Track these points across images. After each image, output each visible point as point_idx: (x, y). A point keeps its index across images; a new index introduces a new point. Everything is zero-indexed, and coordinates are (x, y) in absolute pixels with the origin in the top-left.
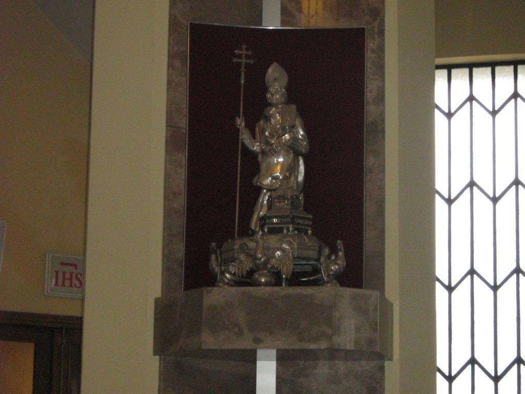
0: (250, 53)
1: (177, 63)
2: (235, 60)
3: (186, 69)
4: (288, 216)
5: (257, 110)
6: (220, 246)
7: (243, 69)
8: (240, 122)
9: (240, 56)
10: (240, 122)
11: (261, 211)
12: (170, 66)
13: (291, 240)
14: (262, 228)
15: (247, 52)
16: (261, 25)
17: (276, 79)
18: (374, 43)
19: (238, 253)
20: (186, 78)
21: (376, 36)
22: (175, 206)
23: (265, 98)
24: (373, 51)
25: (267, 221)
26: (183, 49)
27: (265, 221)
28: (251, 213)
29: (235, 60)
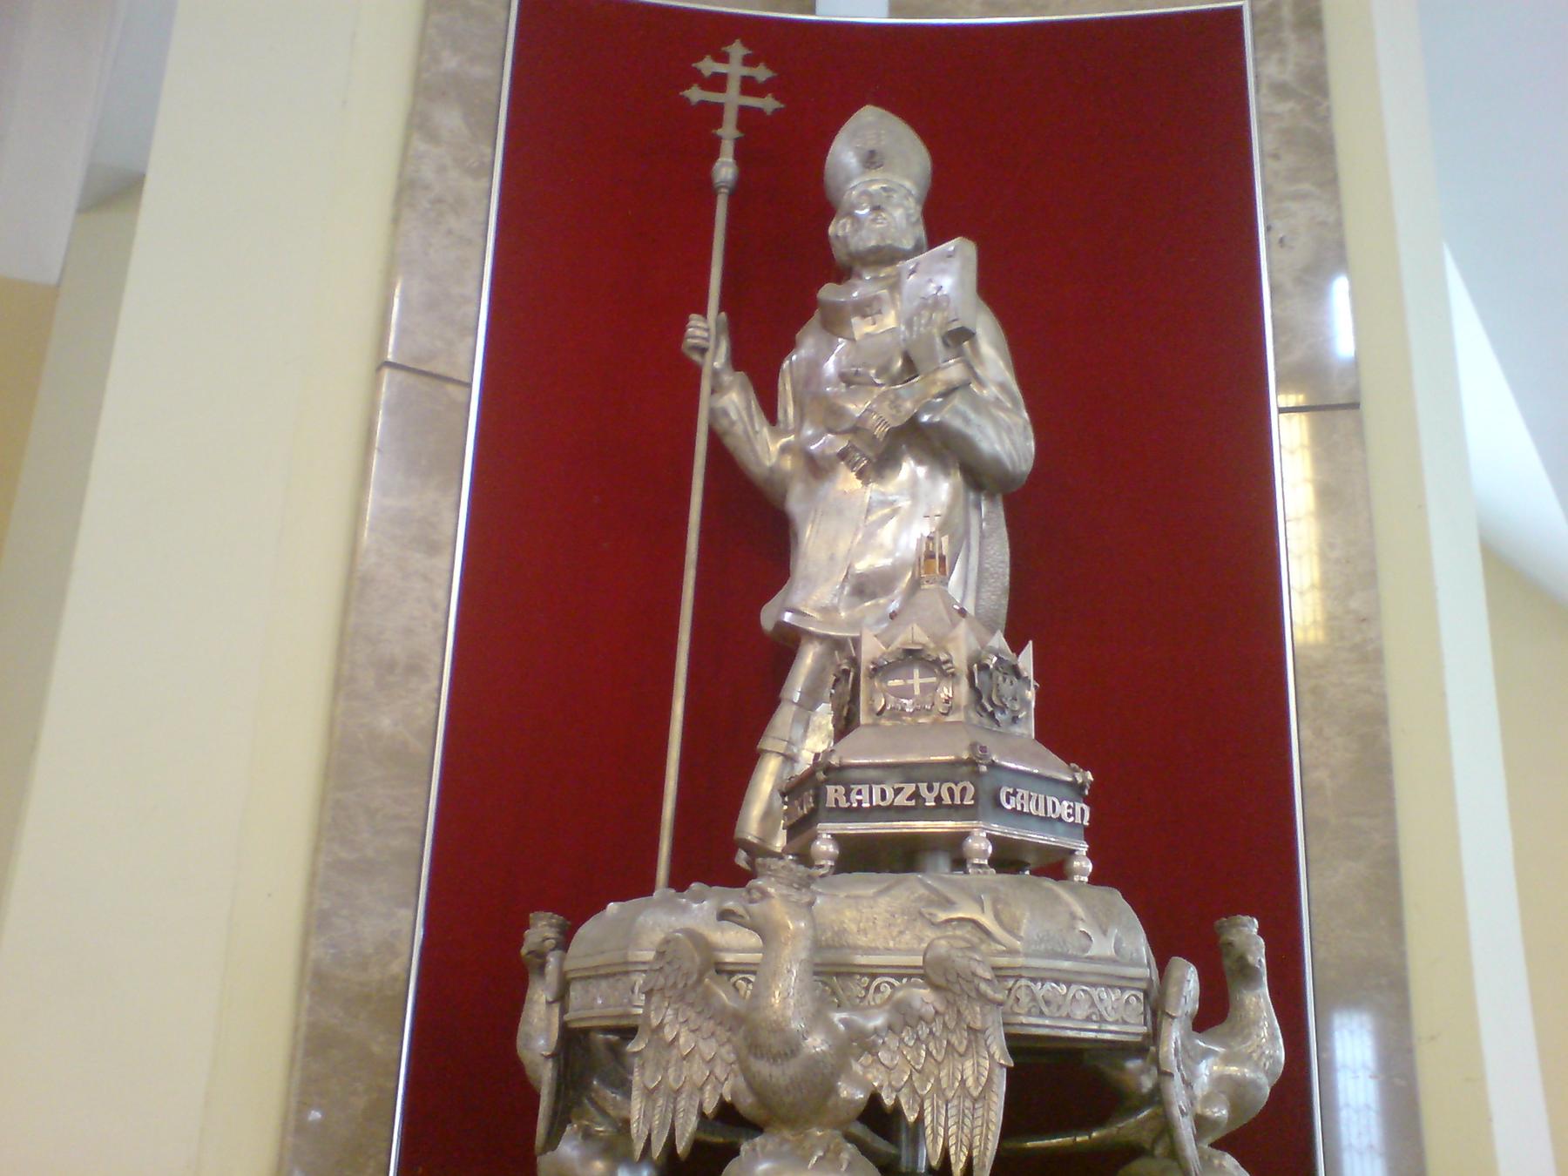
0: (762, 73)
1: (450, 119)
2: (695, 94)
3: (489, 151)
4: (949, 771)
5: (789, 275)
6: (565, 939)
7: (728, 132)
8: (706, 331)
9: (718, 83)
10: (706, 331)
11: (714, 360)
12: (418, 123)
13: (987, 921)
14: (800, 828)
15: (746, 71)
16: (813, 11)
17: (877, 171)
18: (1282, 61)
19: (649, 994)
20: (483, 183)
21: (1288, 35)
22: (385, 723)
23: (824, 241)
24: (1281, 90)
25: (833, 793)
26: (479, 71)
27: (819, 796)
28: (749, 761)
29: (695, 94)
